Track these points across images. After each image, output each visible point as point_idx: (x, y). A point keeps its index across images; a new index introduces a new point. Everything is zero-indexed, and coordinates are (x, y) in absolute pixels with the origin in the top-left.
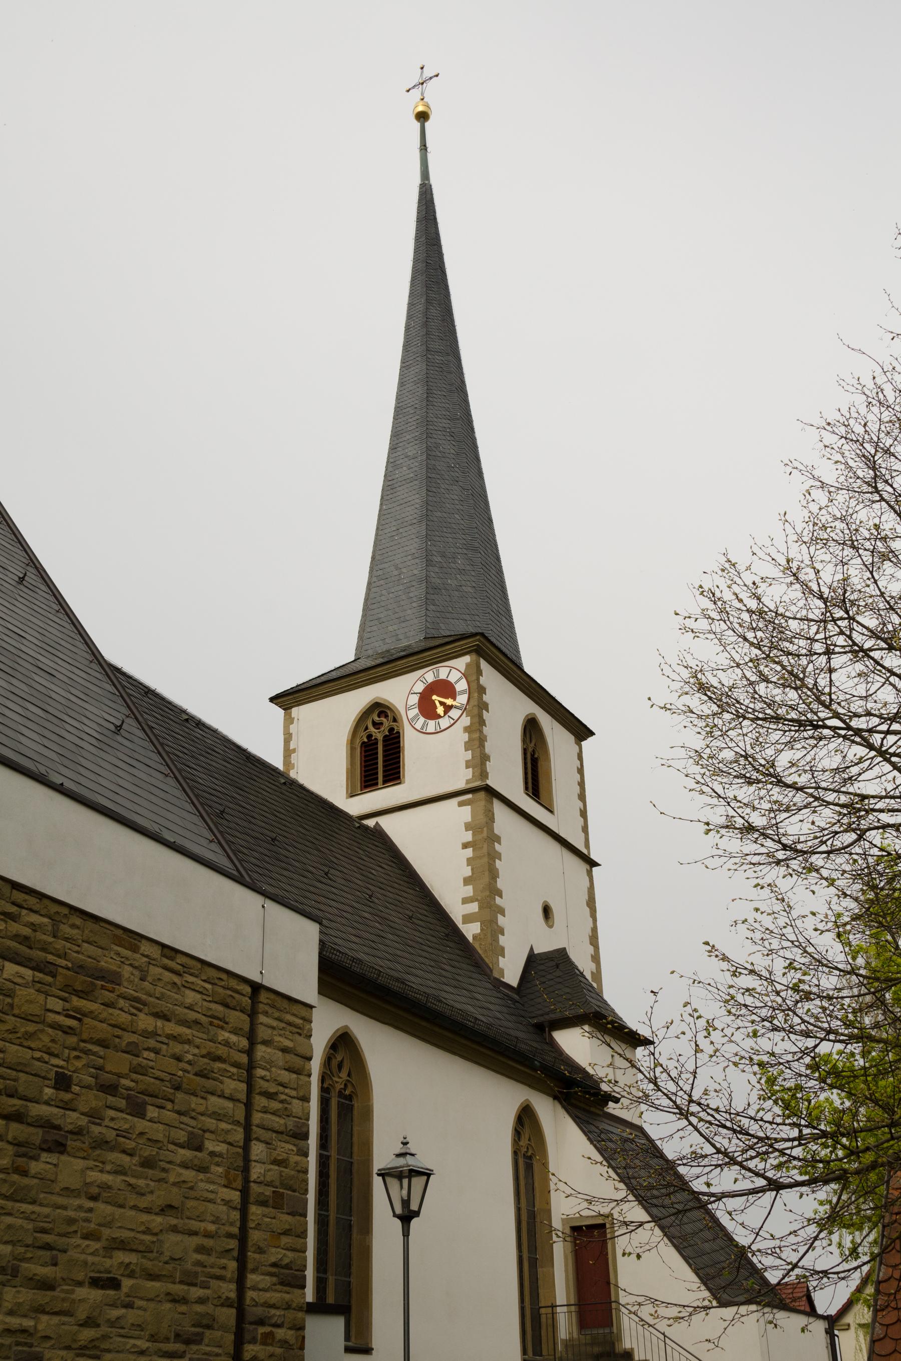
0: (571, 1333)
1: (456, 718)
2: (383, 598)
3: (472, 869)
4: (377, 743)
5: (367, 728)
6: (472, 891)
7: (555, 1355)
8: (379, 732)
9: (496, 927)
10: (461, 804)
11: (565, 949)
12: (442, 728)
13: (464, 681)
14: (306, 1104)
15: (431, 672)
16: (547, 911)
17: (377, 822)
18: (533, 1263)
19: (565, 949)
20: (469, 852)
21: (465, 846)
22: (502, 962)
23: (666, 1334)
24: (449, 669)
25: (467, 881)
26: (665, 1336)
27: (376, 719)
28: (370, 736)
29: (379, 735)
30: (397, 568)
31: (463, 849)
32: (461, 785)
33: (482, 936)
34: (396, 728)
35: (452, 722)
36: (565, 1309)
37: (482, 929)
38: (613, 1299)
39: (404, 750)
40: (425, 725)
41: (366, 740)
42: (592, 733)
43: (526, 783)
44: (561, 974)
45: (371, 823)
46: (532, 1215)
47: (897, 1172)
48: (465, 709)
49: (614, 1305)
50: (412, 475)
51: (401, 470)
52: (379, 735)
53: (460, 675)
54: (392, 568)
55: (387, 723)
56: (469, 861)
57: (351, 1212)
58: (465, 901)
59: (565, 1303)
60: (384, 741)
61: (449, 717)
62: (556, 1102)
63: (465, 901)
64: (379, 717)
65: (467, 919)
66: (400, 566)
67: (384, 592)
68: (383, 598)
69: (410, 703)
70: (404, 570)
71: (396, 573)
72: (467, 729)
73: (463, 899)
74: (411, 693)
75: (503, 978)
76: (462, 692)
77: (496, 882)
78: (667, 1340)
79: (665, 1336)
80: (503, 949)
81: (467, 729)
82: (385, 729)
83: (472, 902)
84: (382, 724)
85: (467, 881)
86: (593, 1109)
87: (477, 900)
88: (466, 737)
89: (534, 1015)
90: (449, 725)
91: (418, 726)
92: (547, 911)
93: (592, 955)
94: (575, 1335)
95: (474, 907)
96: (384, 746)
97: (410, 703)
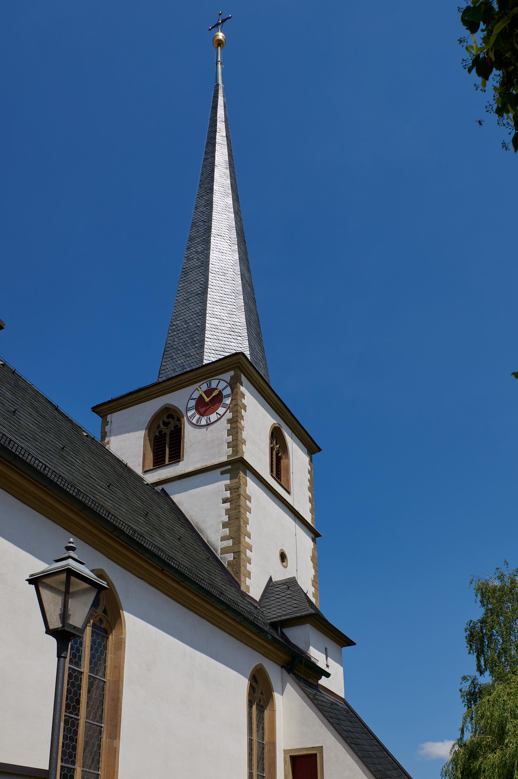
1: (222, 414)
2: (175, 343)
4: (165, 437)
5: (159, 426)
6: (228, 532)
8: (167, 429)
9: (245, 557)
10: (222, 473)
12: (212, 421)
13: (229, 388)
14: (249, 699)
15: (206, 384)
16: (283, 557)
17: (163, 488)
20: (228, 505)
21: (225, 501)
22: (248, 582)
24: (218, 381)
25: (225, 525)
27: (166, 420)
28: (160, 432)
29: (167, 431)
30: (186, 323)
32: (224, 459)
33: (234, 563)
34: (179, 425)
35: (219, 416)
39: (184, 438)
40: (199, 420)
41: (158, 434)
42: (320, 450)
43: (272, 468)
45: (159, 488)
47: (498, 727)
48: (229, 407)
50: (199, 263)
51: (192, 261)
52: (167, 431)
53: (226, 384)
54: (183, 323)
55: (173, 423)
56: (227, 511)
58: (223, 539)
60: (170, 434)
61: (217, 413)
62: (284, 670)
63: (223, 539)
64: (168, 418)
65: (225, 550)
66: (188, 321)
67: (176, 339)
68: (175, 343)
69: (190, 405)
70: (191, 324)
71: (185, 326)
72: (229, 421)
74: (190, 399)
75: (249, 593)
76: (228, 396)
80: (249, 573)
81: (229, 421)
82: (172, 427)
83: (228, 539)
84: (169, 423)
85: (225, 525)
86: (310, 680)
87: (232, 538)
88: (229, 426)
90: (216, 419)
91: (194, 421)
92: (283, 557)
93: (313, 593)
96: (170, 438)
97: (190, 405)
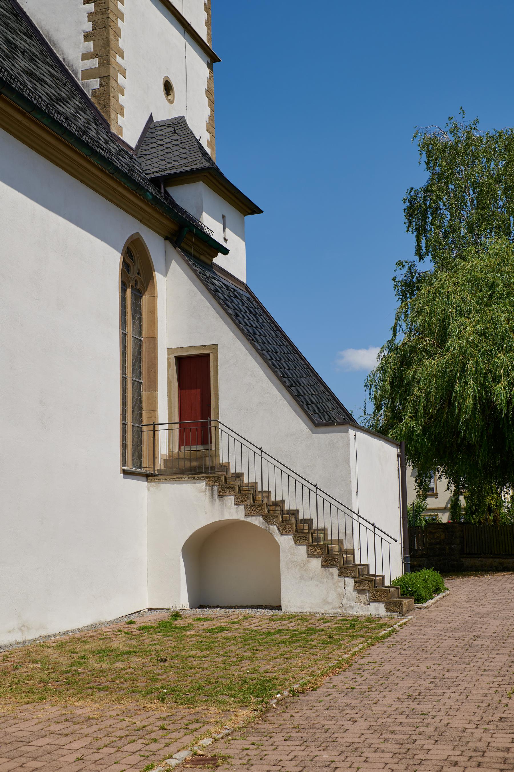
0: (171, 450)
3: (93, 25)
6: (92, 47)
7: (154, 467)
11: (183, 117)
16: (168, 88)
18: (138, 386)
19: (183, 117)
23: (375, 525)
25: (87, 37)
26: (317, 488)
31: (84, 4)
36: (166, 427)
37: (101, 86)
38: (212, 419)
44: (179, 137)
46: (138, 344)
49: (213, 424)
57: (141, 376)
58: (85, 57)
59: (167, 422)
63: (85, 57)
65: (88, 74)
73: (83, 55)
75: (122, 136)
77: (118, 40)
78: (264, 455)
79: (317, 488)
80: (122, 108)
83: (92, 58)
86: (202, 257)
87: (97, 56)
89: (150, 172)
92: (168, 88)
94: (176, 449)
95: (94, 63)
